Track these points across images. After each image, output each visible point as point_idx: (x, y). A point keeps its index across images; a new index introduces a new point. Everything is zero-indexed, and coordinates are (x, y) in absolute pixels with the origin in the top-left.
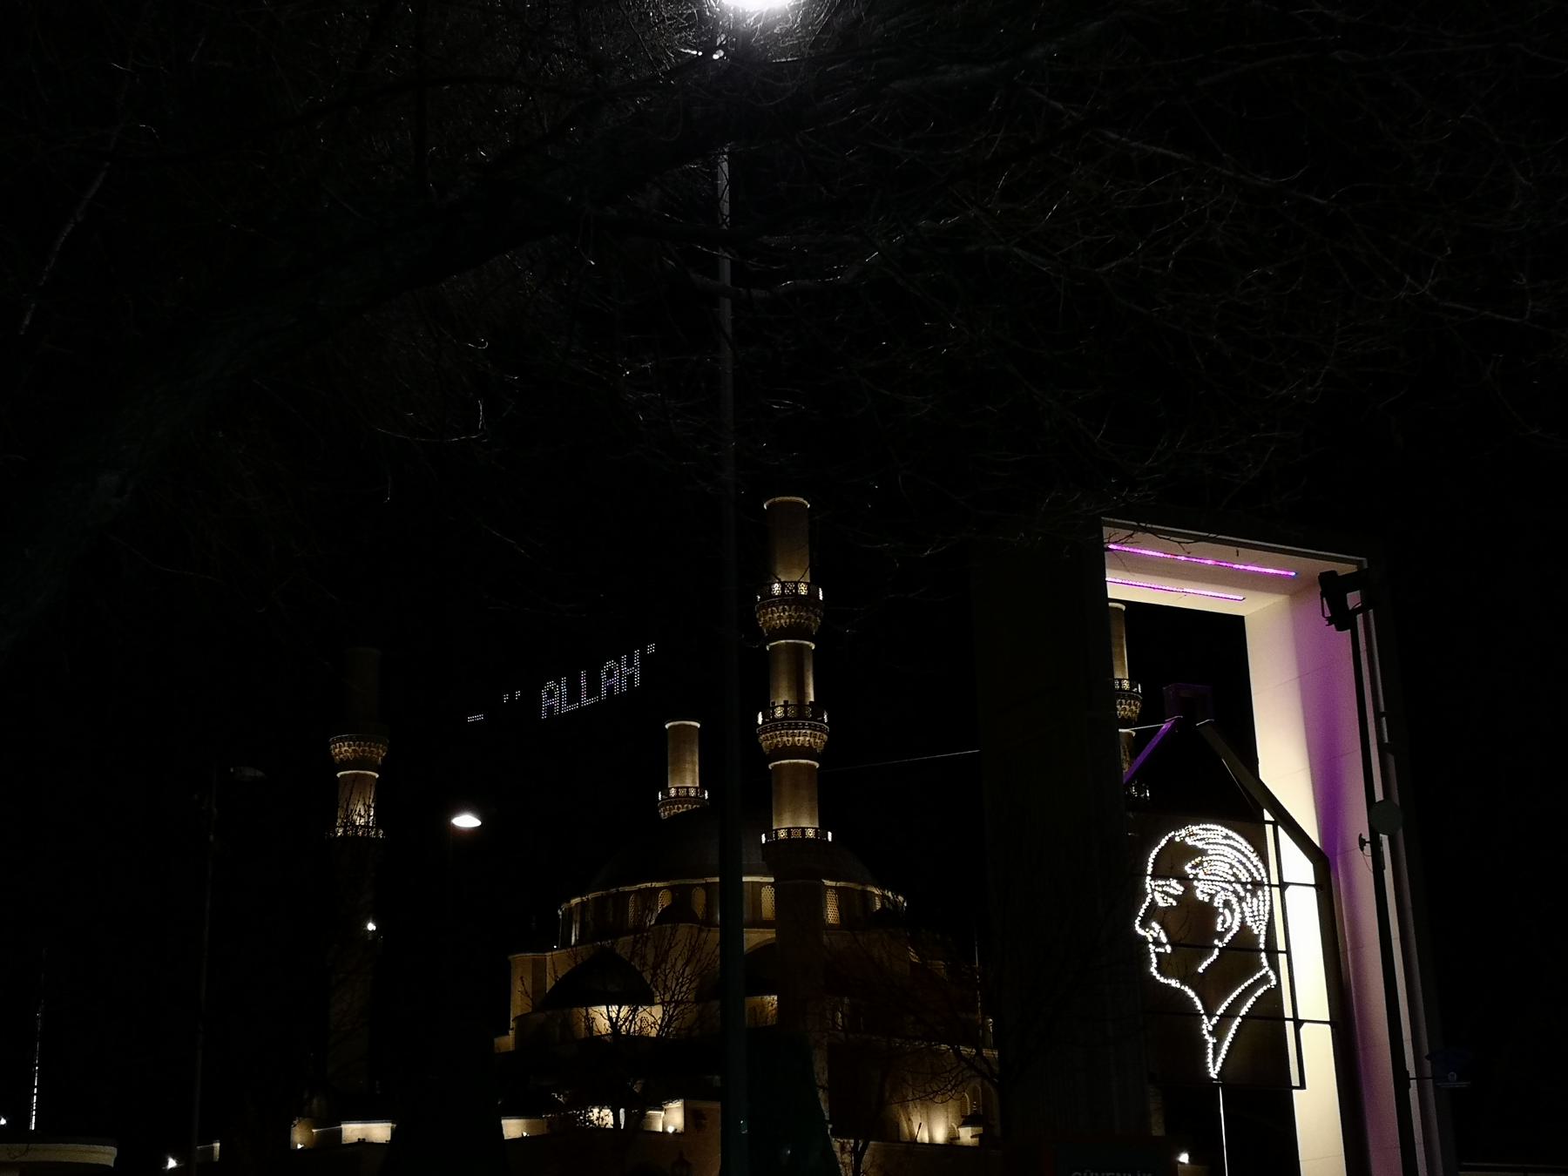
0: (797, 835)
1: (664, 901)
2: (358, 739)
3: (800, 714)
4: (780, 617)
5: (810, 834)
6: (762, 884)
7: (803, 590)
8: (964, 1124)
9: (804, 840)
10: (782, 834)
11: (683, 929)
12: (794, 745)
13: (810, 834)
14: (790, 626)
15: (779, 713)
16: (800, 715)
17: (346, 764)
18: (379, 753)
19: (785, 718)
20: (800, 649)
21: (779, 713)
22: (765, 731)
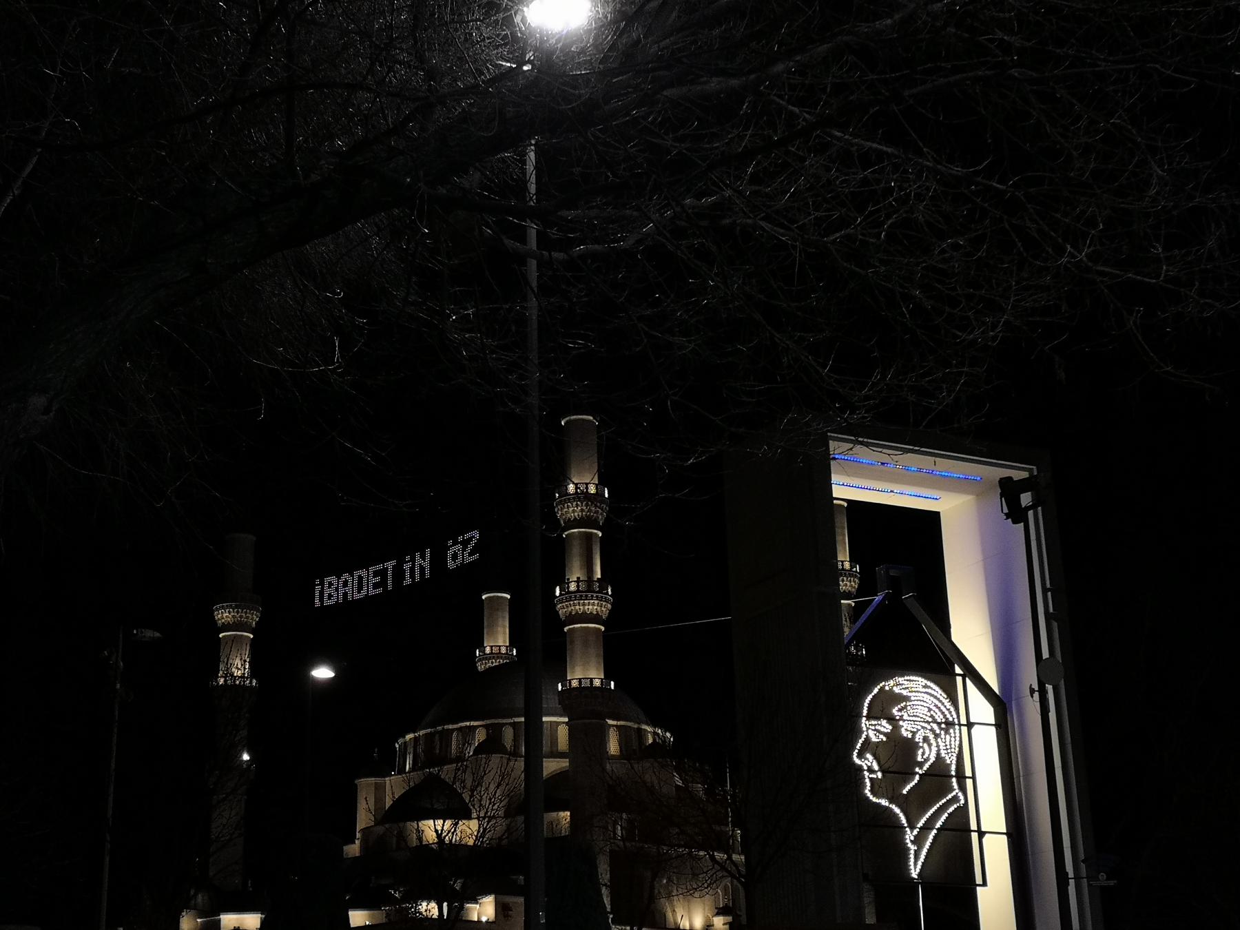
0: (586, 684)
1: (480, 736)
3: (589, 588)
4: (573, 511)
5: (597, 683)
6: (558, 724)
8: (718, 914)
9: (592, 688)
10: (575, 684)
11: (495, 759)
13: (597, 683)
14: (582, 518)
15: (573, 587)
16: (590, 589)
17: (227, 627)
18: (254, 618)
19: (578, 591)
20: (589, 537)
21: (573, 587)
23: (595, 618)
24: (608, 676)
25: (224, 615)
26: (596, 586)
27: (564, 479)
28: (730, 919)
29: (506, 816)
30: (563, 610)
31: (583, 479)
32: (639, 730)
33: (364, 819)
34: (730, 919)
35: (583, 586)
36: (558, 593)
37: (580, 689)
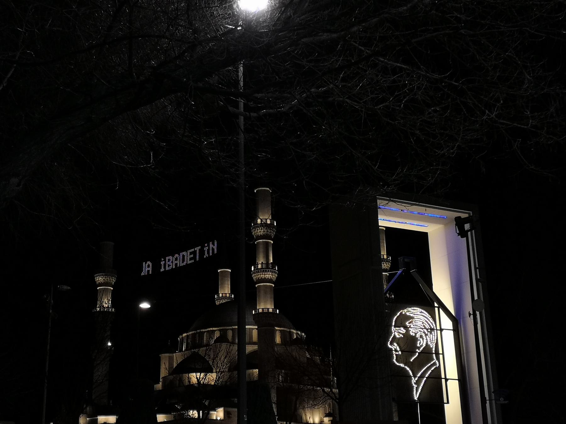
0: (266, 311)
1: (217, 334)
2: (106, 275)
3: (267, 267)
4: (260, 231)
5: (271, 310)
7: (269, 222)
8: (326, 416)
9: (268, 313)
10: (260, 311)
11: (224, 345)
12: (265, 278)
13: (271, 310)
14: (264, 235)
15: (260, 266)
16: (267, 267)
17: (100, 285)
18: (113, 280)
21: (260, 266)
22: (254, 273)
23: (270, 281)
24: (276, 307)
25: (99, 279)
26: (270, 266)
27: (256, 217)
28: (331, 418)
29: (229, 371)
30: (255, 277)
31: (265, 217)
32: (290, 332)
33: (164, 372)
34: (331, 418)
35: (264, 266)
36: (253, 269)
37: (263, 313)
